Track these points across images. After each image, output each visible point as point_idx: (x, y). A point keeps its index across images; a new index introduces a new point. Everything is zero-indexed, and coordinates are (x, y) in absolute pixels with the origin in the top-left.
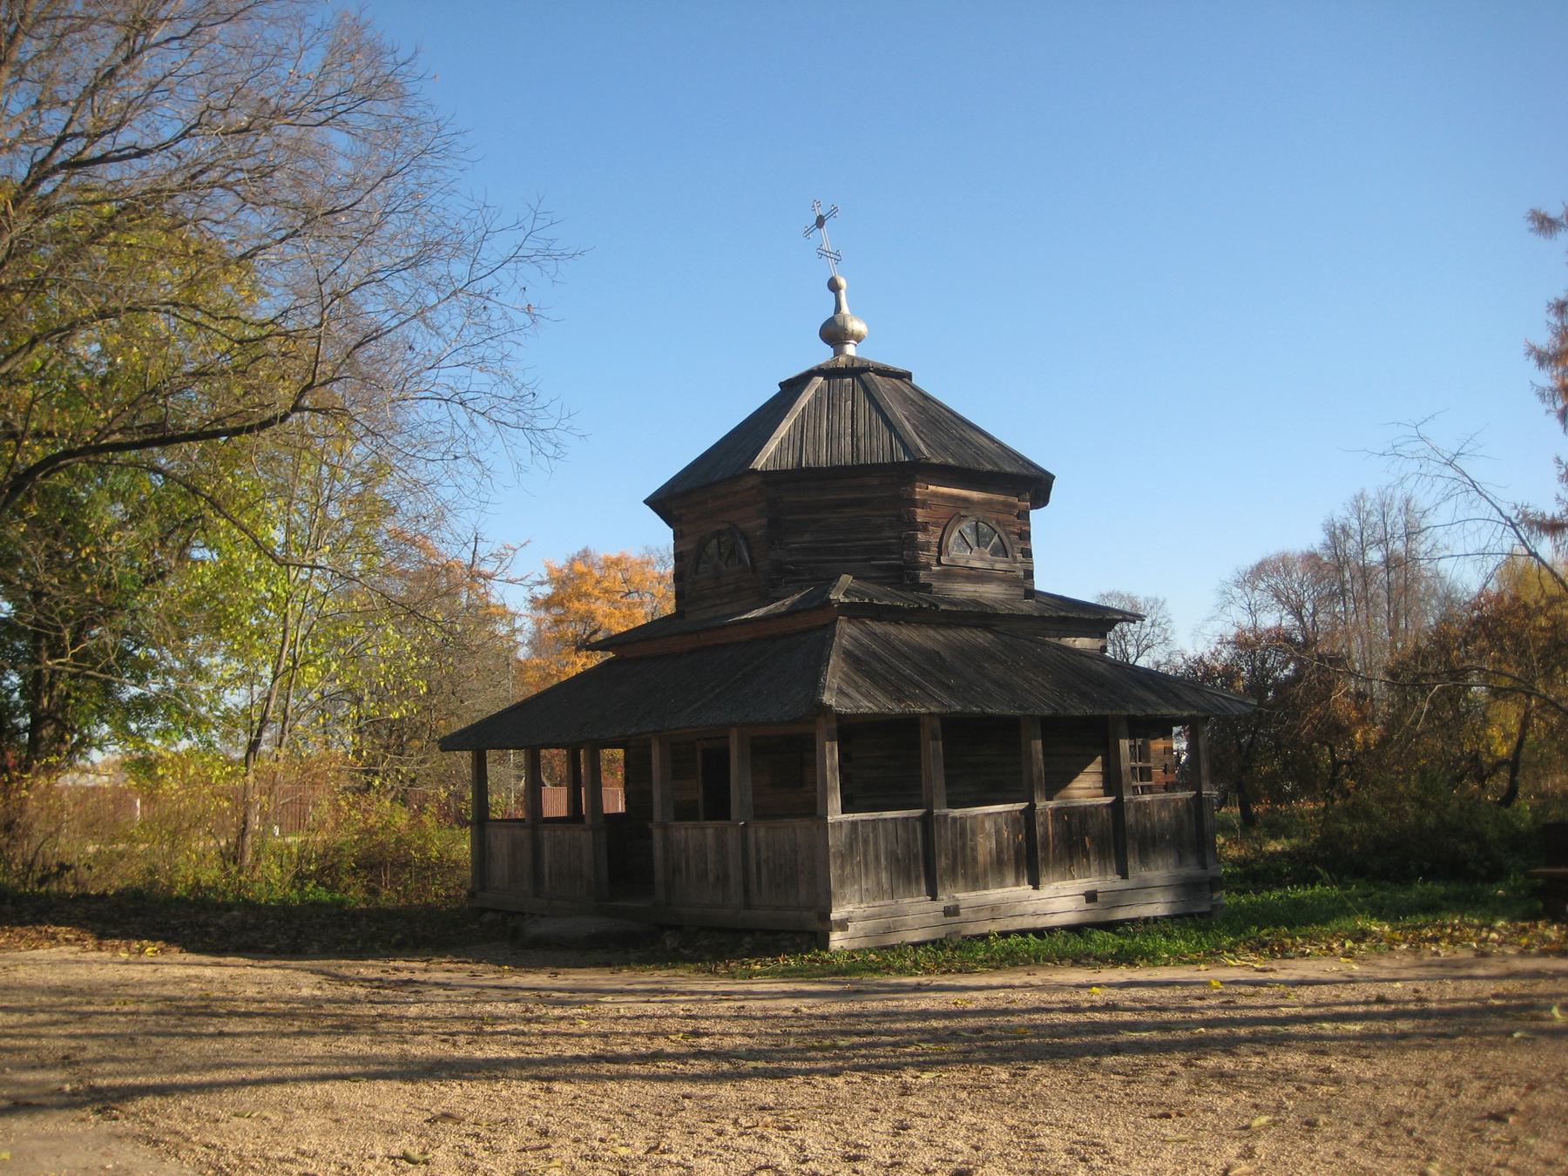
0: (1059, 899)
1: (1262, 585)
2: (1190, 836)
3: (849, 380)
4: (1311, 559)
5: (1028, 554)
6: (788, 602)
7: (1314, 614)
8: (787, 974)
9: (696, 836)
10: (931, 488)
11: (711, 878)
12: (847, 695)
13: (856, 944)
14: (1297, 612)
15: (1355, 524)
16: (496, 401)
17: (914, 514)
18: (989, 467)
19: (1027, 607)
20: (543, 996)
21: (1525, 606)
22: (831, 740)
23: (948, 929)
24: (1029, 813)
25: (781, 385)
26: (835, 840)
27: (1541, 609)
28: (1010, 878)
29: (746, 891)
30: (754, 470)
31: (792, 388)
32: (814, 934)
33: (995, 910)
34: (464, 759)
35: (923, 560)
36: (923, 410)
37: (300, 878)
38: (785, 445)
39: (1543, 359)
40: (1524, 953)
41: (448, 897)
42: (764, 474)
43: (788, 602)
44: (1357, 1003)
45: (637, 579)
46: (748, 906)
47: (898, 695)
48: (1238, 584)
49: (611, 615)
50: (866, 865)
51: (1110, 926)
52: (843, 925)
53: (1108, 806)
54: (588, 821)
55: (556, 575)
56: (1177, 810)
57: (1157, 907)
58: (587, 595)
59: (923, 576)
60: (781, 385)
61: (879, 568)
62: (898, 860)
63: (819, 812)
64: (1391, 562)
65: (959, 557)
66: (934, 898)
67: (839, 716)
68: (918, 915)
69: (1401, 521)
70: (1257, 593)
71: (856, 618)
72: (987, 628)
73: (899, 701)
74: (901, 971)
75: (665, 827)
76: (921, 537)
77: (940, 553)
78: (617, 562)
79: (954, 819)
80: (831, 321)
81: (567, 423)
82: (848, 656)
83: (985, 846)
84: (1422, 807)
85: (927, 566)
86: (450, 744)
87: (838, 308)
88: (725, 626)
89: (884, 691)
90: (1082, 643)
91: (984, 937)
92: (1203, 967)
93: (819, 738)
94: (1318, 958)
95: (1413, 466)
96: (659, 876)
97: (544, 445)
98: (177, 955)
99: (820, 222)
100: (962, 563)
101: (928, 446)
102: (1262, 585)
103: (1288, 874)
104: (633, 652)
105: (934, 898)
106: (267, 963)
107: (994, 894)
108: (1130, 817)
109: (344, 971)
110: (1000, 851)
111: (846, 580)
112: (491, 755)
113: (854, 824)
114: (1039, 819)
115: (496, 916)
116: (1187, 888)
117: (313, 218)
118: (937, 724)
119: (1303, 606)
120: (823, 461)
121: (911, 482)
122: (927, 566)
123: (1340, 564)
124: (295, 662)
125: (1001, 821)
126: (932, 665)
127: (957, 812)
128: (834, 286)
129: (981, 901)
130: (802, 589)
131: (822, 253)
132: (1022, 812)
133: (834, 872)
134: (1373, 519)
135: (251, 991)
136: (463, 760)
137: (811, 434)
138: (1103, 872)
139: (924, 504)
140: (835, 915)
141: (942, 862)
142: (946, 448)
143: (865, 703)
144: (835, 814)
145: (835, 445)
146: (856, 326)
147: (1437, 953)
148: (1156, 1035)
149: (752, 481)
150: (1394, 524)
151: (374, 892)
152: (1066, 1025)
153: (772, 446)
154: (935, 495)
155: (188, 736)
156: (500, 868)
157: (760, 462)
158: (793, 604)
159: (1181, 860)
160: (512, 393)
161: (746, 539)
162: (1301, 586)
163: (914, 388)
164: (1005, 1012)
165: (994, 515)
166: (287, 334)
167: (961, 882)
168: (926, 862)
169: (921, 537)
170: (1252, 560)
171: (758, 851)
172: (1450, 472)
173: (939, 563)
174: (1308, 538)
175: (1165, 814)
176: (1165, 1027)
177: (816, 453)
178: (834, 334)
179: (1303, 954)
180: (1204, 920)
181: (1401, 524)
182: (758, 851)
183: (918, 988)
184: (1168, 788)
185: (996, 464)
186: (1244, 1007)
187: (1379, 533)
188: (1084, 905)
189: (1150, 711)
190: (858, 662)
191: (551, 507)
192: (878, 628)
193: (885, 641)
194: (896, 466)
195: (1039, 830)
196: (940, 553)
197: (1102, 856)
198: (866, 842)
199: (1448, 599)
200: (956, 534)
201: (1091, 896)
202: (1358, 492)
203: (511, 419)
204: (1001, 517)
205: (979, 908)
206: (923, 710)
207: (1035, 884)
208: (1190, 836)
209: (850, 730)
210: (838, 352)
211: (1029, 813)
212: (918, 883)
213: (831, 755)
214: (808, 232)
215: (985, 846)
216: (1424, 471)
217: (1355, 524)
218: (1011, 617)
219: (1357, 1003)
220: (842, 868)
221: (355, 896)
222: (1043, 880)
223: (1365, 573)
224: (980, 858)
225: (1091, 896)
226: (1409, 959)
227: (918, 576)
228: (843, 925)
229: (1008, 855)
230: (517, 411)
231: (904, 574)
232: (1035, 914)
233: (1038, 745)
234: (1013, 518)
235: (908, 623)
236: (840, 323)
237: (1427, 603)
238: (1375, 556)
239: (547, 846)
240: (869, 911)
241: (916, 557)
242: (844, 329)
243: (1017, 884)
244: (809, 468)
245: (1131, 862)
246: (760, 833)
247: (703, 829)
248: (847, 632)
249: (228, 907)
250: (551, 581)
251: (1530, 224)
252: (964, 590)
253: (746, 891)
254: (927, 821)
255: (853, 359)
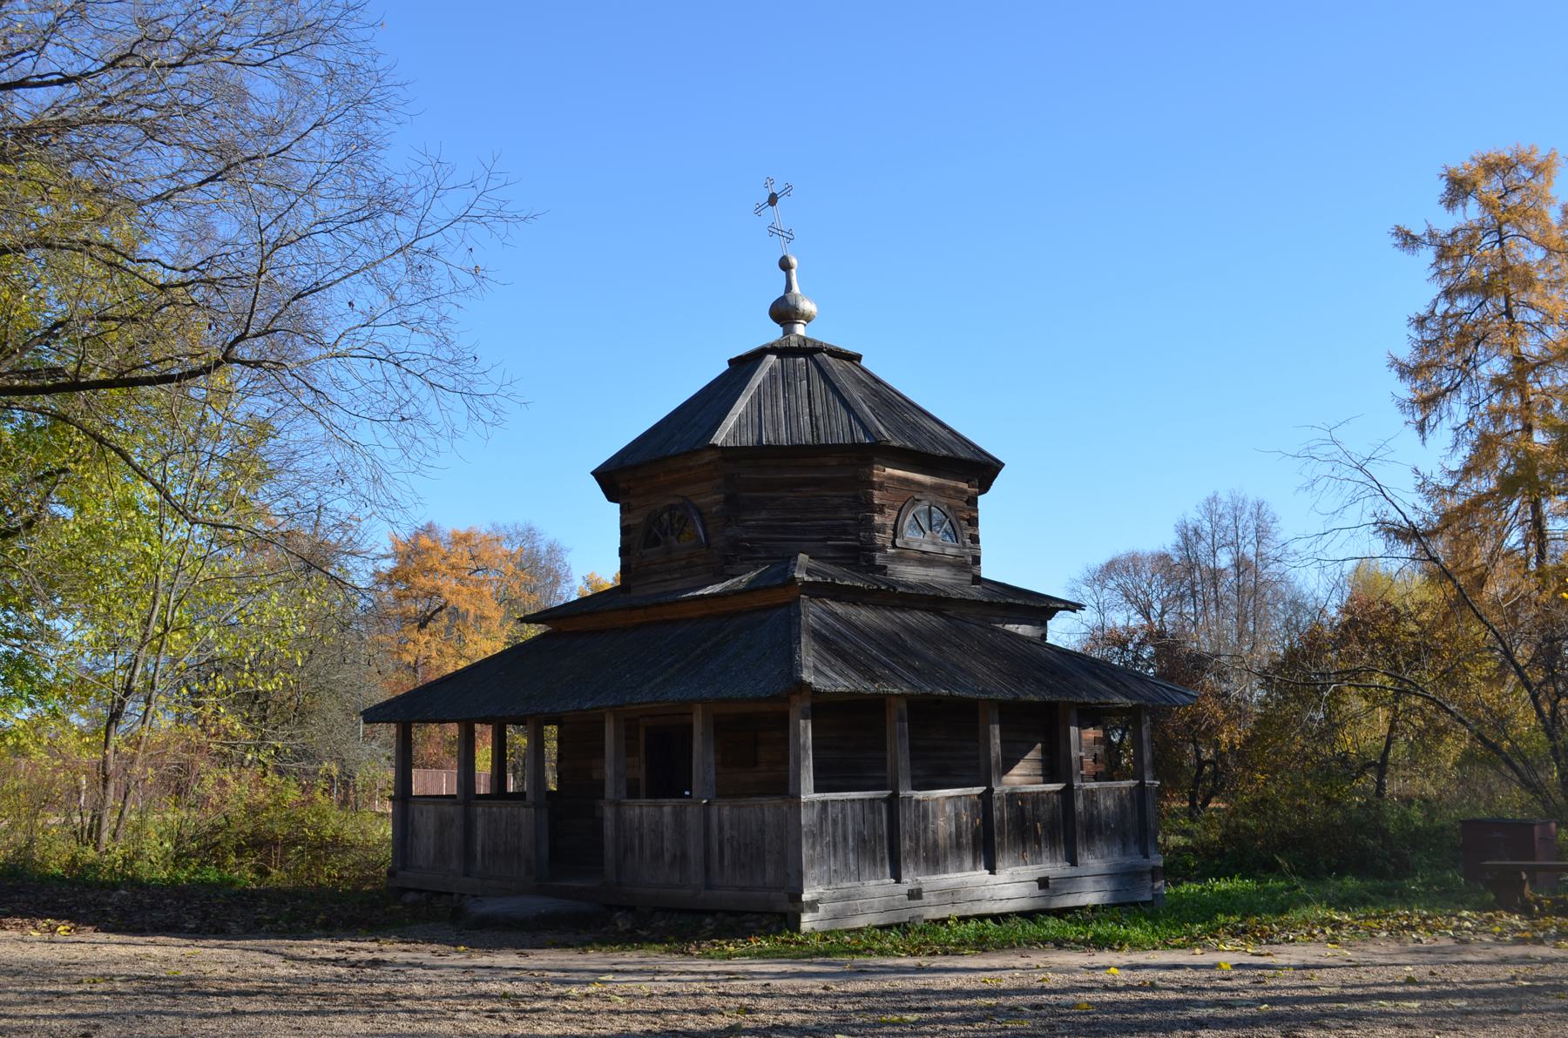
0: (1007, 885)
1: (1112, 584)
2: (1133, 825)
3: (802, 359)
4: (1163, 559)
5: (975, 539)
6: (745, 578)
7: (1163, 613)
8: (762, 955)
9: (650, 815)
10: (889, 470)
11: (667, 856)
12: (822, 673)
13: (825, 926)
14: (1145, 612)
15: (1207, 526)
16: (432, 363)
17: (872, 495)
18: (945, 452)
19: (975, 592)
20: (539, 977)
21: (1396, 611)
22: (805, 718)
23: (911, 913)
24: (987, 797)
25: (731, 362)
26: (807, 818)
27: (1411, 615)
28: (968, 862)
29: (707, 870)
30: (715, 446)
31: (743, 366)
32: (784, 915)
33: (953, 894)
34: (388, 732)
35: (879, 542)
36: (876, 393)
37: (180, 859)
38: (744, 421)
39: (1405, 371)
40: (1499, 939)
41: (341, 878)
42: (724, 449)
43: (745, 578)
44: (1394, 984)
45: (486, 556)
46: (709, 887)
47: (869, 674)
48: (1087, 582)
49: (459, 593)
50: (835, 846)
51: (1060, 913)
52: (813, 906)
53: (1057, 792)
54: (530, 797)
55: (401, 548)
56: (1121, 799)
57: (1090, 896)
58: (432, 570)
59: (879, 559)
60: (731, 362)
61: (835, 548)
62: (864, 841)
63: (791, 789)
64: (1240, 564)
65: (912, 543)
66: (898, 881)
67: (816, 693)
68: (876, 896)
69: (1252, 525)
70: (1106, 591)
71: (817, 597)
72: (937, 612)
73: (873, 681)
74: (881, 952)
75: (618, 805)
76: (878, 519)
77: (895, 536)
78: (465, 538)
79: (918, 801)
80: (783, 300)
81: (509, 389)
82: (816, 635)
83: (943, 826)
84: (1327, 804)
85: (883, 548)
86: (373, 715)
87: (789, 287)
88: (679, 601)
89: (858, 671)
90: (1024, 630)
91: (944, 921)
92: (1198, 951)
93: (793, 716)
94: (1304, 944)
95: (1325, 469)
96: (609, 852)
97: (482, 410)
98: (89, 934)
99: (773, 200)
100: (915, 546)
101: (887, 429)
102: (1112, 584)
103: (1195, 868)
104: (573, 627)
105: (898, 881)
106: (205, 942)
107: (951, 878)
108: (1080, 805)
109: (295, 951)
110: (959, 834)
111: (803, 558)
112: (417, 733)
113: (824, 803)
114: (996, 804)
115: (426, 892)
116: (1124, 878)
117: (227, 166)
118: (903, 705)
119: (1150, 605)
120: (784, 439)
121: (869, 464)
122: (883, 548)
123: (1191, 566)
124: (166, 628)
125: (960, 804)
126: (893, 646)
127: (920, 795)
128: (785, 265)
129: (943, 885)
130: (756, 567)
131: (773, 230)
132: (979, 796)
133: (806, 851)
134: (1225, 522)
135: (222, 971)
136: (387, 732)
137: (768, 412)
138: (1053, 858)
139: (881, 487)
140: (806, 896)
141: (906, 845)
142: (902, 433)
143: (841, 680)
144: (808, 794)
145: (794, 425)
146: (807, 306)
147: (1419, 941)
148: (1220, 1012)
149: (708, 456)
150: (1246, 528)
151: (262, 872)
152: (1130, 1003)
153: (730, 421)
154: (891, 477)
155: (31, 704)
156: (425, 844)
157: (720, 438)
158: (751, 582)
159: (1124, 852)
160: (450, 357)
161: (701, 514)
162: (1150, 585)
163: (864, 370)
164: (1043, 991)
165: (945, 501)
166: (212, 282)
167: (922, 865)
168: (890, 844)
169: (878, 519)
170: (1102, 559)
171: (721, 829)
172: (1360, 476)
173: (894, 546)
174: (1157, 537)
175: (1110, 803)
176: (1227, 1005)
177: (776, 431)
178: (784, 313)
179: (1287, 940)
180: (1135, 908)
181: (1252, 528)
182: (721, 829)
183: (919, 969)
184: (1096, 778)
185: (950, 450)
186: (1272, 988)
187: (1230, 537)
188: (1038, 892)
189: (1102, 699)
190: (829, 644)
191: (494, 474)
192: (839, 608)
193: (847, 623)
194: (856, 447)
195: (996, 814)
196: (895, 536)
197: (1053, 843)
198: (835, 822)
199: (1296, 605)
200: (910, 517)
201: (1043, 883)
202: (1211, 495)
203: (449, 382)
204: (952, 502)
205: (942, 892)
206: (896, 691)
207: (992, 869)
208: (1133, 825)
209: (825, 708)
210: (788, 331)
211: (987, 797)
212: (883, 866)
213: (806, 732)
214: (758, 211)
215: (943, 826)
216: (1335, 474)
217: (1207, 526)
218: (963, 602)
219: (1394, 984)
220: (813, 847)
221: (243, 873)
222: (999, 864)
223: (1216, 575)
224: (941, 842)
225: (1043, 883)
226: (1394, 946)
227: (873, 558)
228: (813, 906)
229: (967, 839)
230: (454, 373)
231: (861, 556)
232: (992, 899)
233: (996, 730)
234: (962, 504)
235: (865, 604)
236: (792, 303)
237: (1275, 607)
238: (1224, 559)
239: (480, 824)
240: (837, 894)
241: (872, 539)
242: (796, 308)
243: (975, 868)
244: (769, 446)
245: (1079, 849)
246: (724, 811)
247: (661, 807)
248: (812, 612)
249: (114, 887)
250: (396, 554)
251: (1394, 240)
252: (912, 574)
253: (707, 870)
254: (893, 802)
255: (805, 339)
